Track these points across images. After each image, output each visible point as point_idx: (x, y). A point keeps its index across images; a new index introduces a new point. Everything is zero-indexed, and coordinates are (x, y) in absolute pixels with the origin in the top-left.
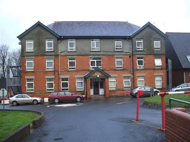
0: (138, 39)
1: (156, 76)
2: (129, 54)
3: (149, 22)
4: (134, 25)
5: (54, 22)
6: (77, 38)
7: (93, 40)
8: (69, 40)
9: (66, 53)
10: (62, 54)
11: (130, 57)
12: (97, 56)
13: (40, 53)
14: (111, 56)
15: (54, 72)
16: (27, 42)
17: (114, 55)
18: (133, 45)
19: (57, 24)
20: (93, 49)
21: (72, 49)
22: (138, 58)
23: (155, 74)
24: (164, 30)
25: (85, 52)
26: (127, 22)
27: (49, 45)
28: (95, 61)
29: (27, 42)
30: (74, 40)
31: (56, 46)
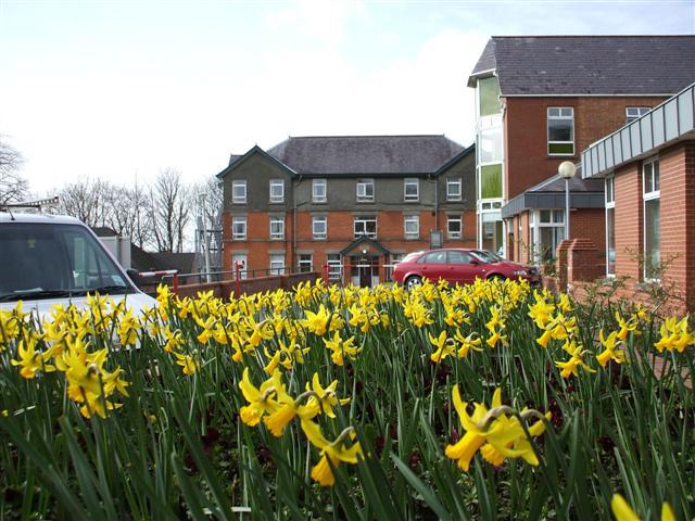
0: (451, 179)
1: (273, 255)
2: (431, 209)
3: (256, 146)
4: (455, 144)
5: (285, 138)
6: (376, 177)
7: (360, 182)
8: (406, 179)
9: (308, 207)
10: (303, 208)
11: (434, 214)
12: (365, 210)
13: (258, 204)
14: (396, 217)
15: (285, 243)
16: (235, 185)
17: (401, 212)
18: (442, 190)
19: (296, 145)
20: (361, 198)
21: (321, 199)
22: (451, 217)
23: (271, 252)
24: (226, 166)
25: (345, 204)
26: (443, 136)
27: (277, 191)
28: (365, 221)
29: (235, 185)
30: (325, 181)
31: (289, 192)
